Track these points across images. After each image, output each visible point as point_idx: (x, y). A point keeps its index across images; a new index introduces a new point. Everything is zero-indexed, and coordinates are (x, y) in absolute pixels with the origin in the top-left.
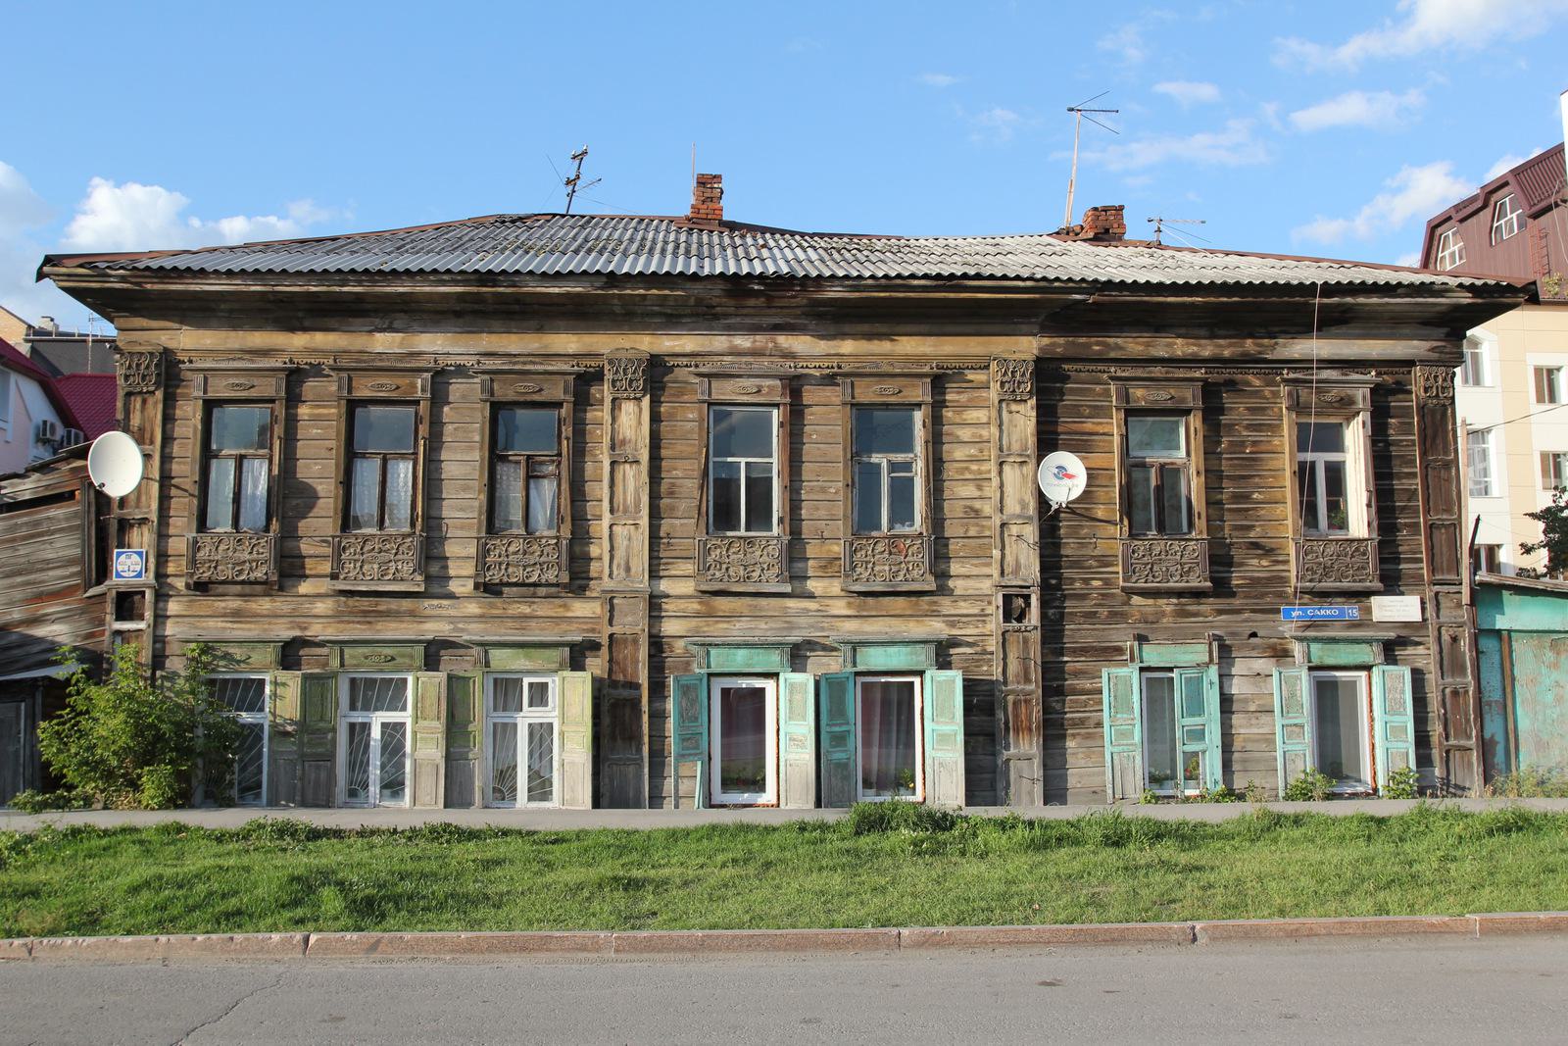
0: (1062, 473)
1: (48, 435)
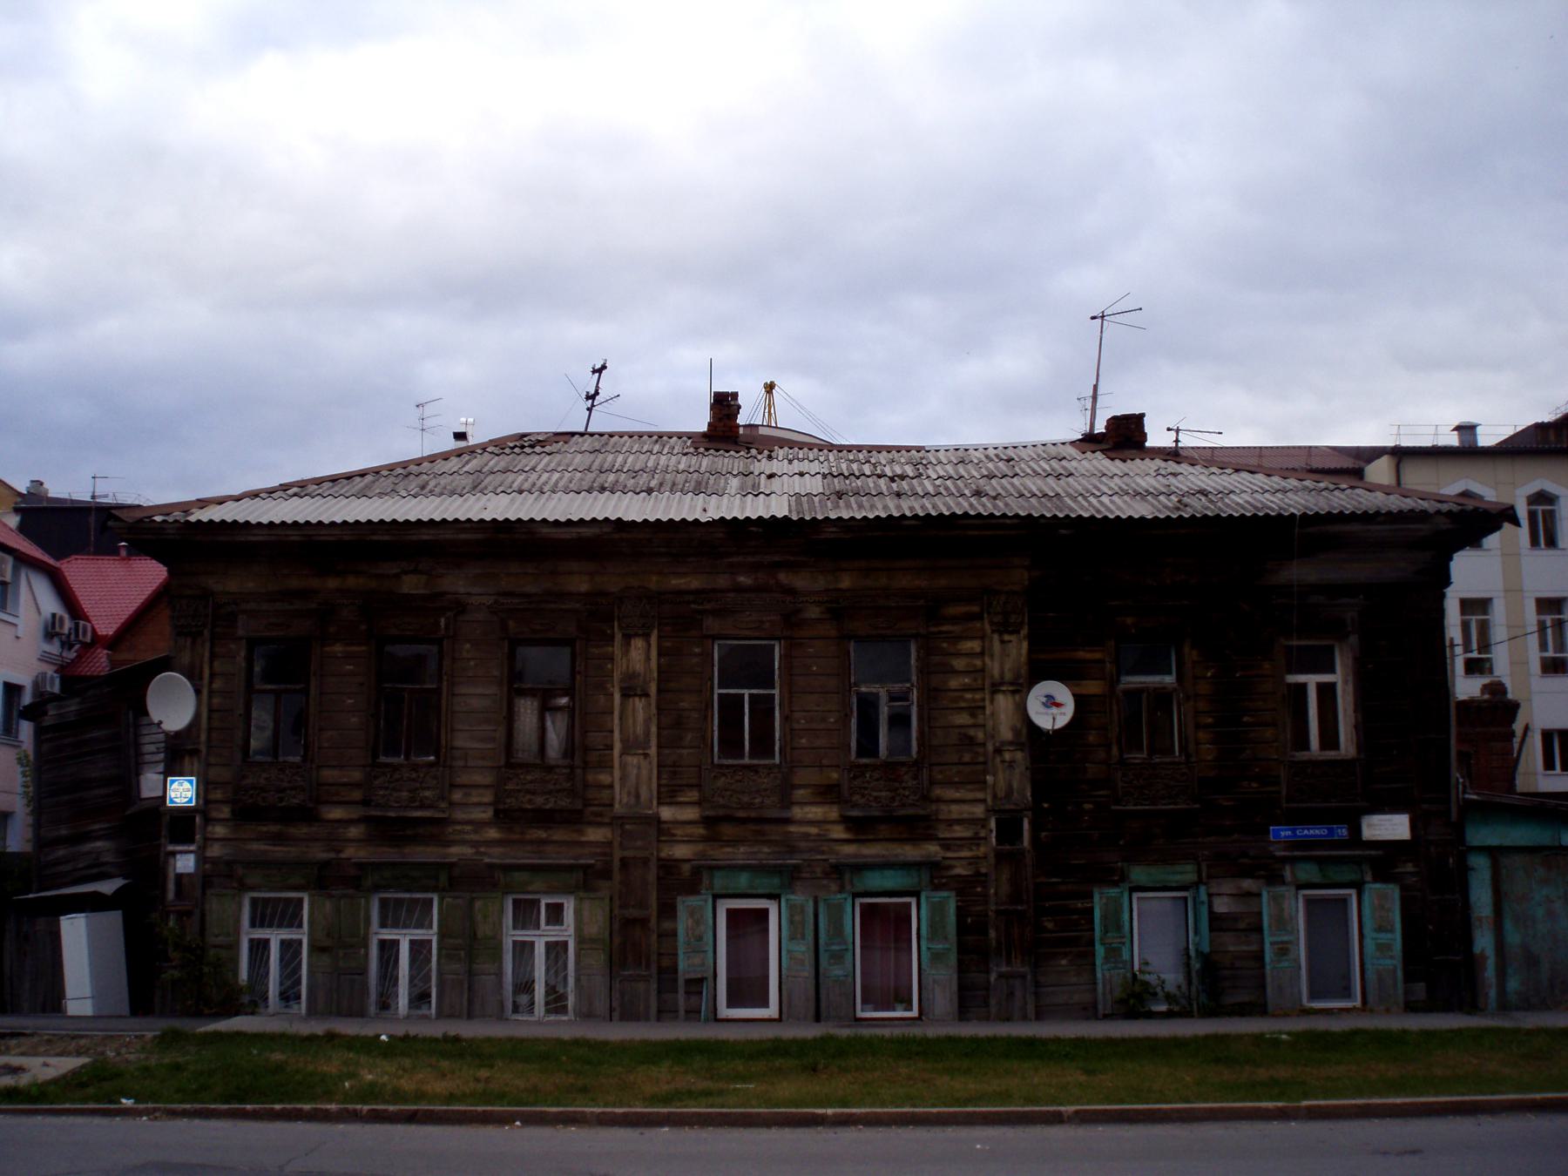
0: (1051, 702)
1: (57, 629)
